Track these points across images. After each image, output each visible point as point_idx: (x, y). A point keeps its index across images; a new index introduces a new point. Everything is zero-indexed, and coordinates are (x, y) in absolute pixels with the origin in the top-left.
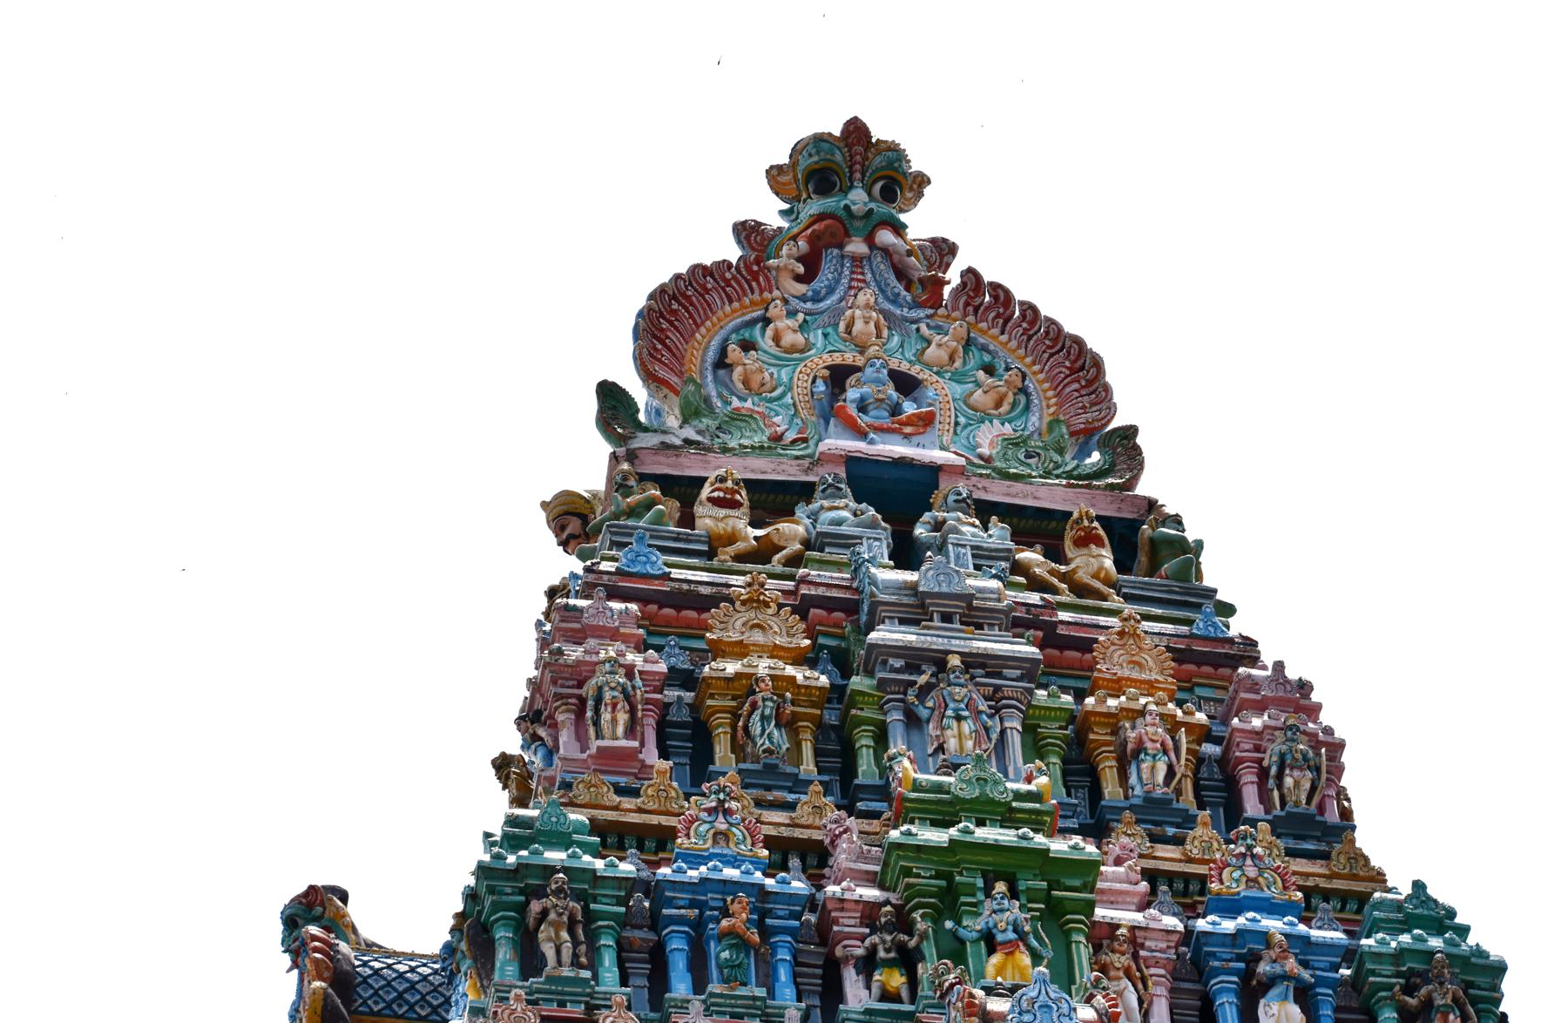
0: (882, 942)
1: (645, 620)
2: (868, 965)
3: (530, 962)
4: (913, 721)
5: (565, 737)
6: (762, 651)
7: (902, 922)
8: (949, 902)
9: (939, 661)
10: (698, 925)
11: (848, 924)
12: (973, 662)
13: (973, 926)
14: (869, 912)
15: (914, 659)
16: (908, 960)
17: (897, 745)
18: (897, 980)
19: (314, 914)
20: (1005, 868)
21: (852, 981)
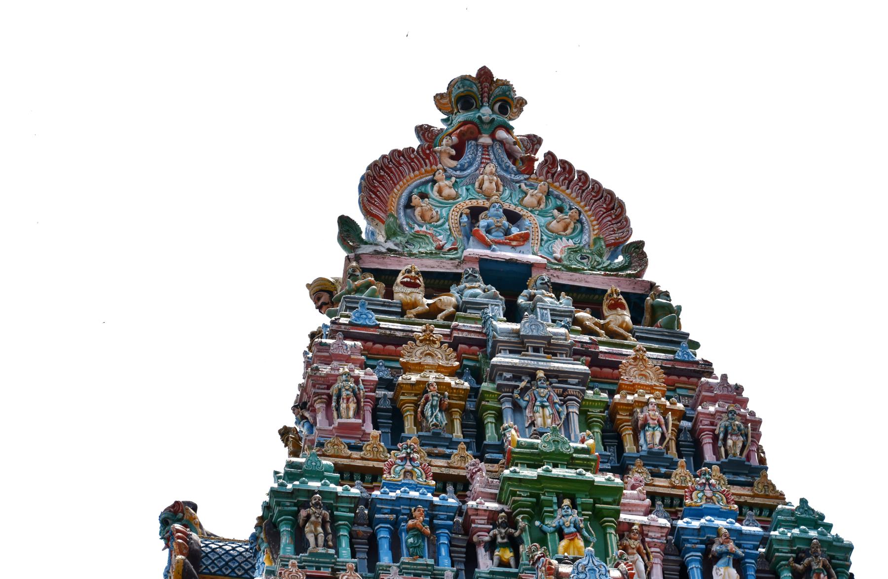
0: (500, 533)
1: (365, 351)
2: (491, 546)
3: (300, 544)
4: (517, 408)
5: (320, 417)
6: (431, 368)
7: (511, 522)
8: (537, 510)
9: (532, 374)
10: (396, 524)
11: (480, 523)
12: (551, 375)
13: (551, 524)
14: (492, 516)
15: (518, 373)
16: (514, 543)
17: (508, 422)
18: (508, 555)
19: (178, 517)
20: (569, 491)
21: (482, 555)
